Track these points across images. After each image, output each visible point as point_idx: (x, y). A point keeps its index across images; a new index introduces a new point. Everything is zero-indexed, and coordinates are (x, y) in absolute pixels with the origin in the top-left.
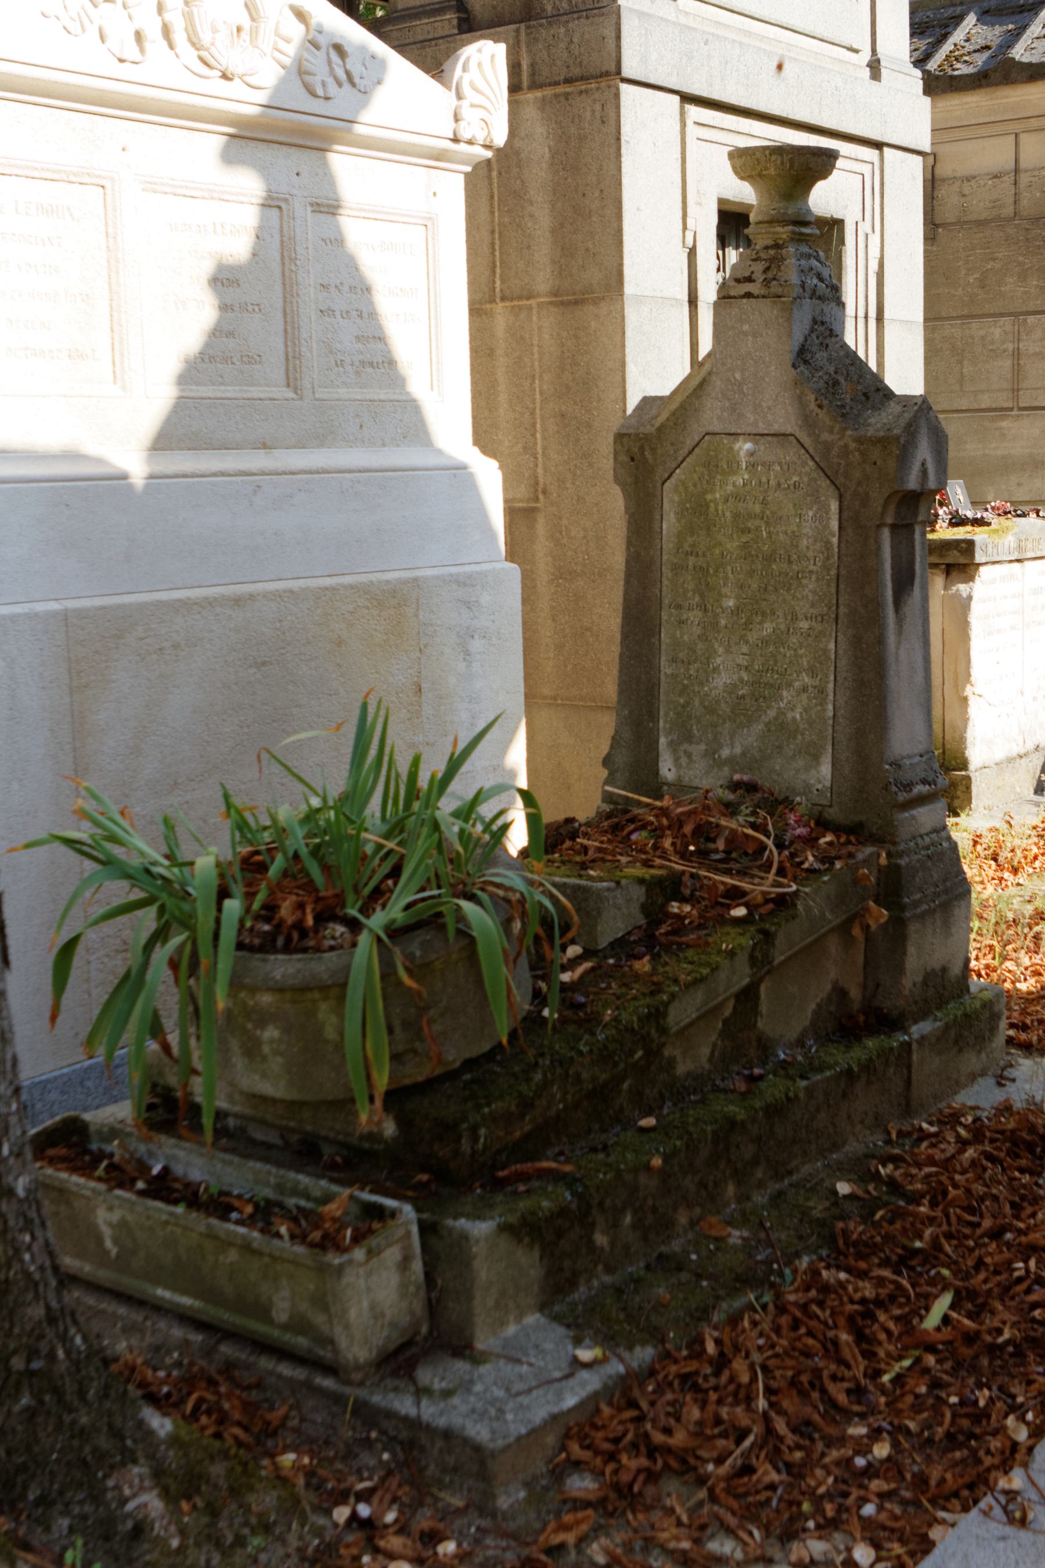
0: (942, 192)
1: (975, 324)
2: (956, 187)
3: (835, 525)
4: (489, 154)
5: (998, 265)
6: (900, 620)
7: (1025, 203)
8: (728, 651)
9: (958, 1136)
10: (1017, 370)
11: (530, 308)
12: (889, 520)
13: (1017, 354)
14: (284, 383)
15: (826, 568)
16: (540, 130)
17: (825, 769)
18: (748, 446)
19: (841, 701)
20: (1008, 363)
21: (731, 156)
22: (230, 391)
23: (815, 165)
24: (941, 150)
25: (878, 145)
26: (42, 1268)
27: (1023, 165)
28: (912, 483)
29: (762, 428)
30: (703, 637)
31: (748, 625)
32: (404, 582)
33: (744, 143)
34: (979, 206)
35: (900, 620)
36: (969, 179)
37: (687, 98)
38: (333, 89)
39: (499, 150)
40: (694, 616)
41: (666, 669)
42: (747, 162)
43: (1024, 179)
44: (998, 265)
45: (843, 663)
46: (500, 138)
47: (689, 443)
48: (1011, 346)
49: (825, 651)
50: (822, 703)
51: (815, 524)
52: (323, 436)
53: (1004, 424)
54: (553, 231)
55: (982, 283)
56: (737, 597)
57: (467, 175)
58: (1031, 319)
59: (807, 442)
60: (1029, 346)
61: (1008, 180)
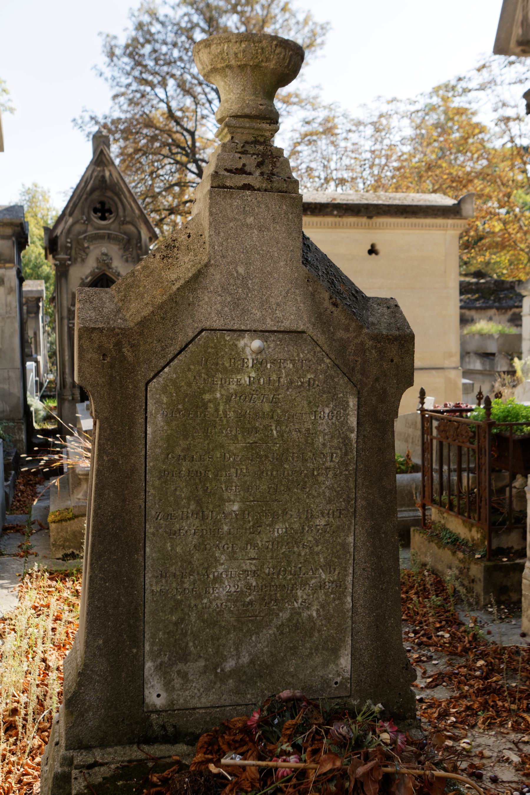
3: (353, 421)
17: (345, 662)
18: (256, 344)
29: (270, 325)
30: (200, 547)
40: (190, 526)
41: (151, 584)
49: (344, 545)
56: (243, 501)
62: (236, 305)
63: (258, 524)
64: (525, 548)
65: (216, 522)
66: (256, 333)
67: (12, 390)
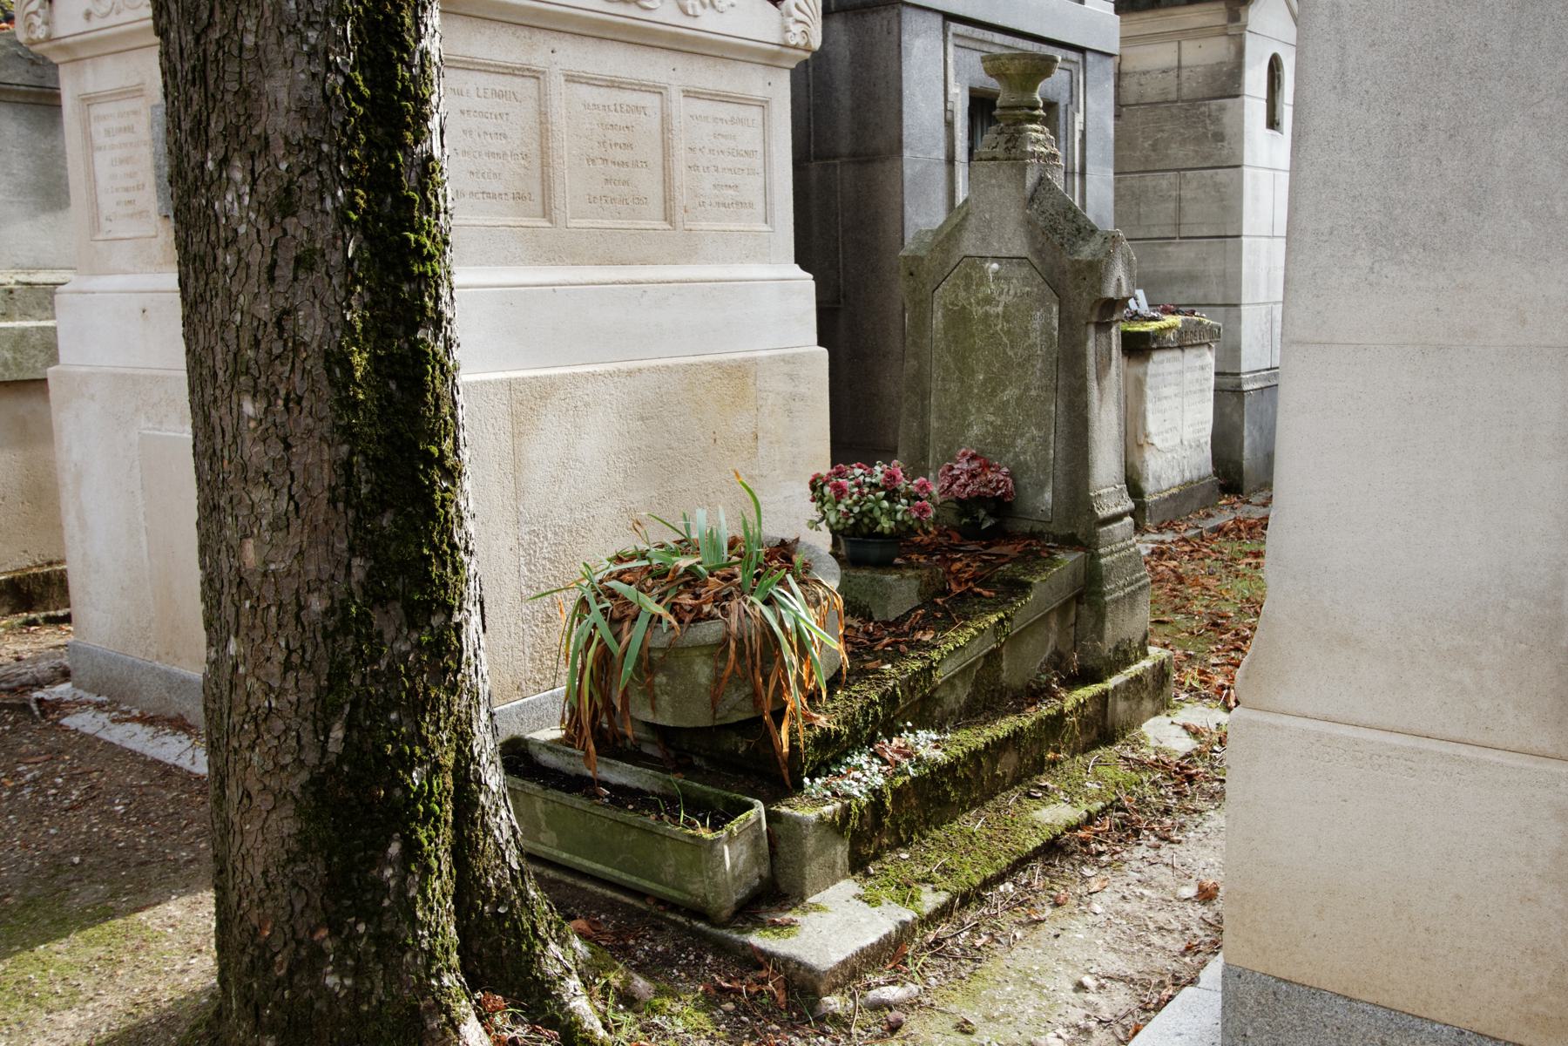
0: (1125, 83)
1: (1149, 176)
2: (1135, 80)
3: (1056, 323)
4: (808, 55)
5: (1165, 135)
6: (1101, 391)
7: (1185, 90)
8: (979, 410)
9: (408, 653)
10: (1179, 209)
11: (835, 166)
12: (1094, 319)
13: (1179, 199)
14: (661, 216)
15: (1049, 353)
16: (843, 39)
17: (1048, 496)
18: (995, 266)
19: (1060, 446)
20: (1172, 205)
21: (983, 60)
22: (626, 224)
23: (1044, 67)
24: (1126, 52)
25: (1082, 50)
26: (508, 842)
27: (1184, 63)
28: (1111, 293)
29: (1004, 253)
30: (961, 401)
31: (994, 393)
32: (746, 361)
33: (996, 50)
34: (1152, 92)
35: (1101, 391)
36: (1145, 73)
37: (949, 17)
38: (699, 10)
39: (814, 53)
40: (953, 387)
41: (934, 423)
42: (994, 65)
43: (1185, 73)
44: (1165, 135)
45: (1061, 420)
46: (816, 43)
47: (953, 263)
48: (1174, 194)
49: (1049, 412)
50: (1046, 449)
51: (1044, 320)
52: (688, 254)
53: (1170, 249)
54: (852, 110)
55: (1154, 147)
56: (986, 373)
57: (792, 70)
58: (1189, 173)
59: (1035, 261)
60: (1187, 193)
61: (1173, 74)
62: (984, 239)
63: (994, 390)
64: (718, 366)
65: (971, 386)
66: (996, 258)
67: (1162, 719)
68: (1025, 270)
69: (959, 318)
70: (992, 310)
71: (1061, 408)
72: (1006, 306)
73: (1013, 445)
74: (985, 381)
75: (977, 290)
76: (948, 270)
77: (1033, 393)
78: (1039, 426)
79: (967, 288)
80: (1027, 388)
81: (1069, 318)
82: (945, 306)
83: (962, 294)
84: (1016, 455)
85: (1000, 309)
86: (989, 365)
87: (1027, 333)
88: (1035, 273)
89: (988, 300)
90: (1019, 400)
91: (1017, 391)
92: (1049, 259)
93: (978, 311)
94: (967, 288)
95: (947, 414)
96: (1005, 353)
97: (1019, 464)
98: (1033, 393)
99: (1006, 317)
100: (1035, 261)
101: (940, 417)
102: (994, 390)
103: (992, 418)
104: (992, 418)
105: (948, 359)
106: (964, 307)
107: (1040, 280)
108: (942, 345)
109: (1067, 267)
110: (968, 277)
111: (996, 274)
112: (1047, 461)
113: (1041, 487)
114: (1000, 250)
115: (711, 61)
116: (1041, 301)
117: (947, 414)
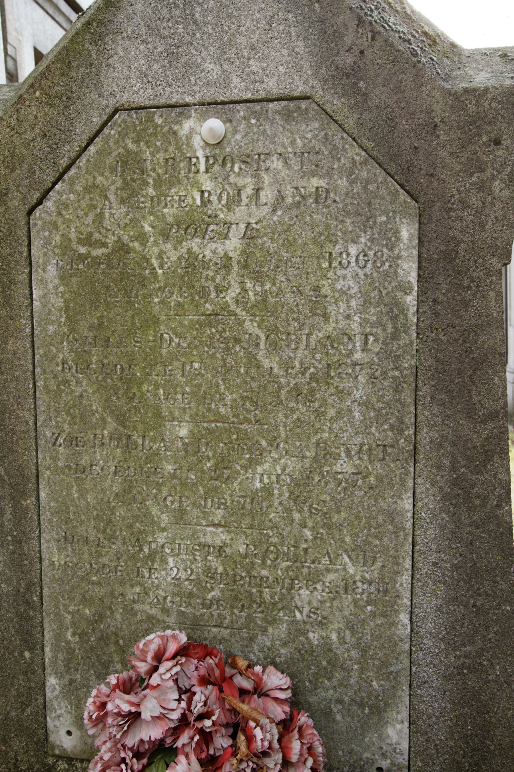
3: (409, 271)
8: (180, 517)
17: (397, 733)
18: (215, 125)
19: (427, 604)
29: (238, 88)
40: (103, 459)
41: (53, 554)
45: (429, 534)
47: (82, 131)
49: (392, 516)
56: (195, 419)
62: (173, 56)
63: (223, 463)
65: (153, 456)
66: (211, 106)
68: (309, 131)
69: (110, 278)
70: (209, 250)
71: (430, 500)
72: (250, 235)
73: (286, 603)
74: (196, 439)
75: (161, 199)
76: (69, 150)
77: (344, 466)
78: (362, 553)
79: (129, 195)
80: (325, 454)
81: (449, 257)
82: (65, 247)
83: (116, 212)
84: (298, 631)
85: (233, 245)
86: (202, 398)
87: (318, 307)
88: (338, 137)
89: (195, 224)
90: (300, 490)
91: (293, 465)
92: (380, 95)
93: (165, 255)
94: (129, 195)
95: (88, 530)
96: (253, 362)
97: (307, 653)
98: (344, 466)
99: (252, 264)
100: (336, 103)
101: (67, 539)
102: (223, 463)
103: (221, 537)
104: (221, 537)
105: (83, 387)
106: (122, 249)
107: (355, 153)
108: (65, 352)
109: (439, 110)
110: (130, 163)
111: (219, 154)
112: (393, 643)
113: (377, 710)
114: (225, 80)
115: (18, 65)
116: (363, 214)
117: (88, 530)
